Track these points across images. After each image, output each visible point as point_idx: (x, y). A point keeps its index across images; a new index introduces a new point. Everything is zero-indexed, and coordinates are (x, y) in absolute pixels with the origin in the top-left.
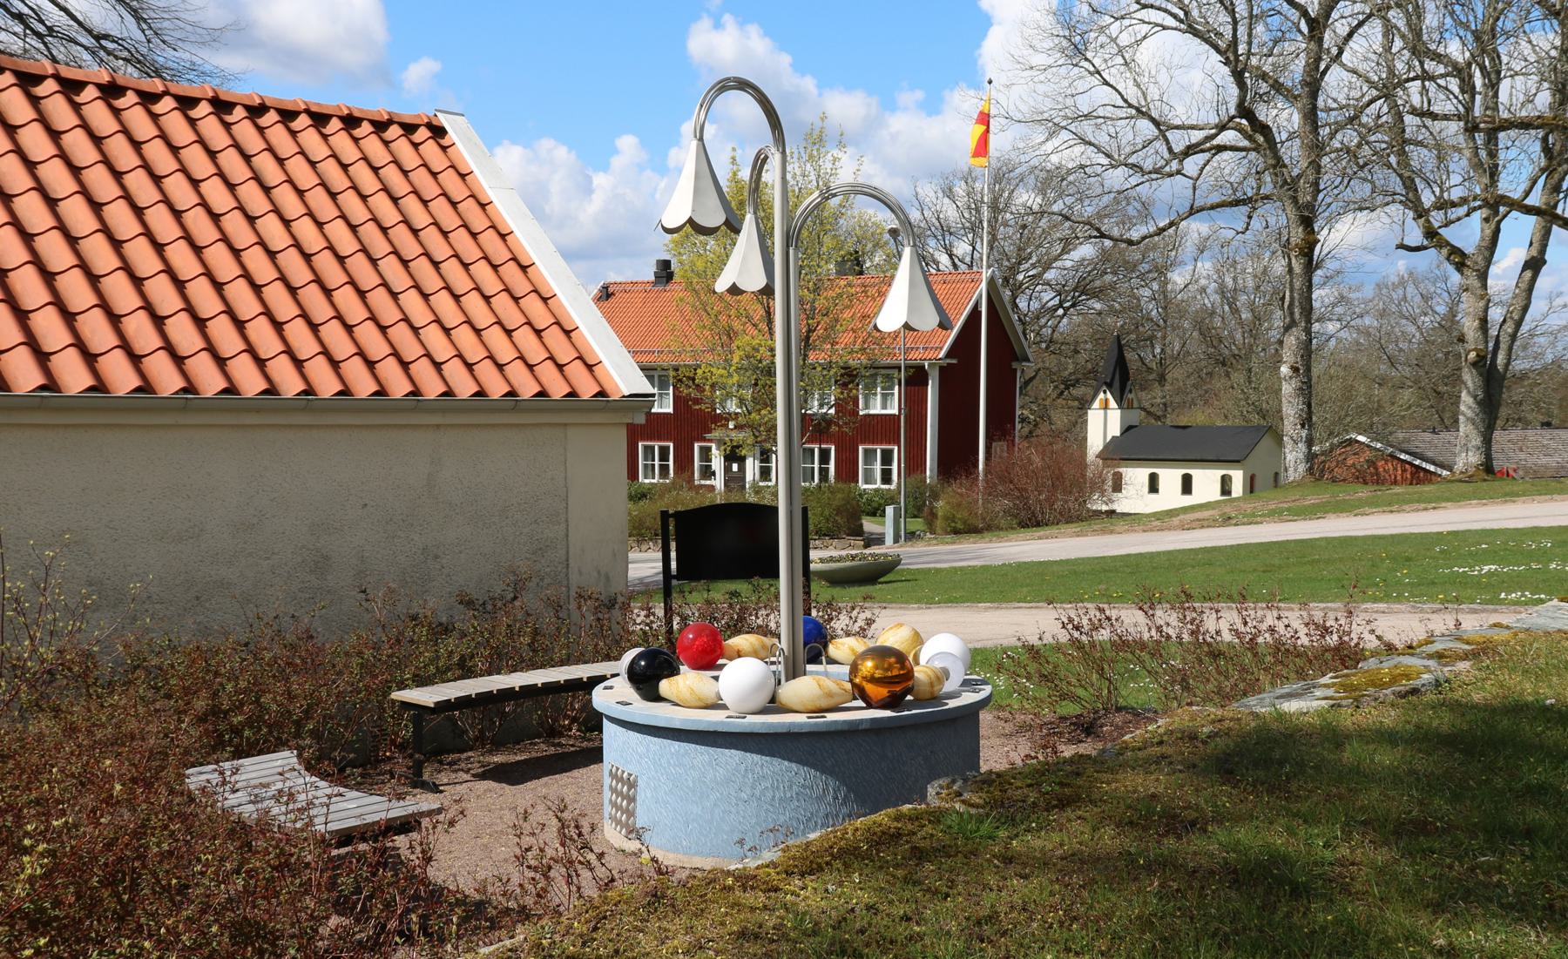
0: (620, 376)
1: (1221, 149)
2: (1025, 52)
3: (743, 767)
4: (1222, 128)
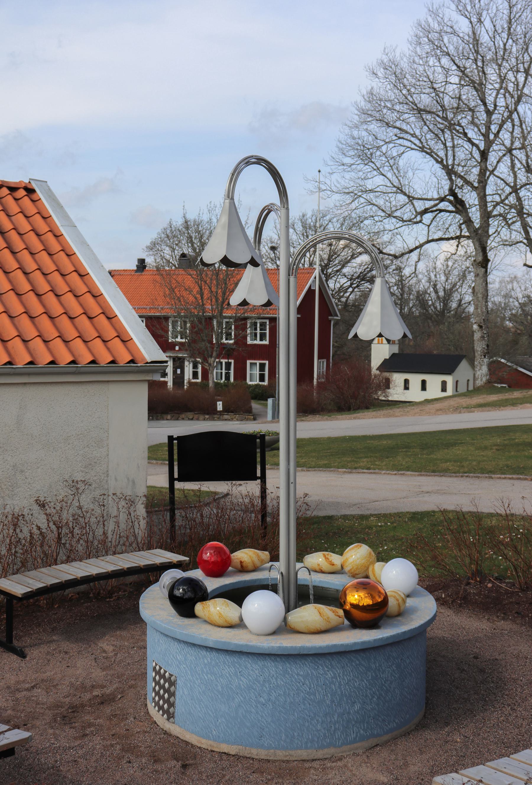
0: (144, 348)
1: (441, 211)
2: (341, 157)
3: (261, 679)
4: (442, 200)
